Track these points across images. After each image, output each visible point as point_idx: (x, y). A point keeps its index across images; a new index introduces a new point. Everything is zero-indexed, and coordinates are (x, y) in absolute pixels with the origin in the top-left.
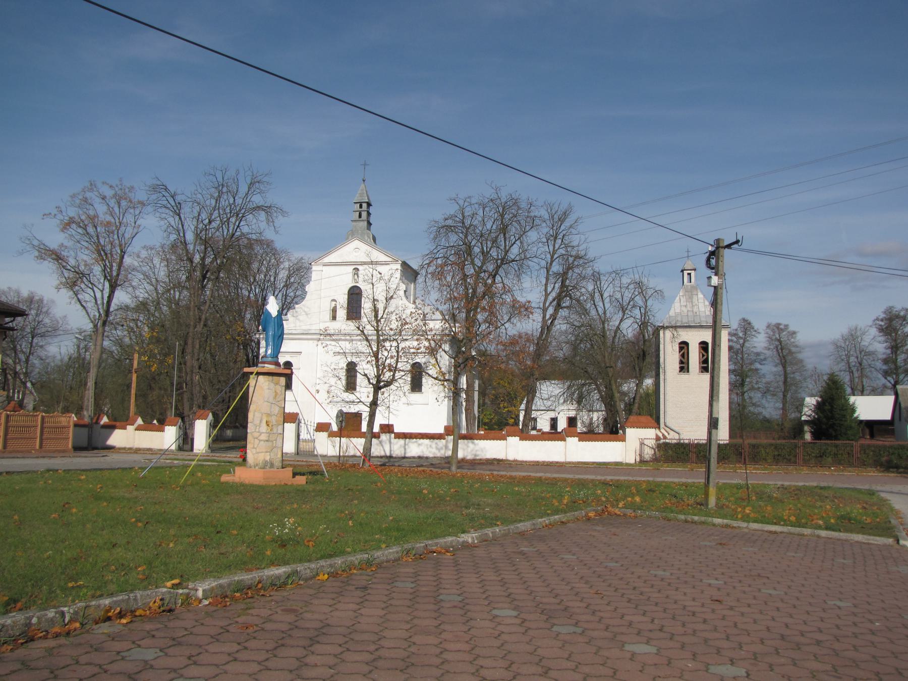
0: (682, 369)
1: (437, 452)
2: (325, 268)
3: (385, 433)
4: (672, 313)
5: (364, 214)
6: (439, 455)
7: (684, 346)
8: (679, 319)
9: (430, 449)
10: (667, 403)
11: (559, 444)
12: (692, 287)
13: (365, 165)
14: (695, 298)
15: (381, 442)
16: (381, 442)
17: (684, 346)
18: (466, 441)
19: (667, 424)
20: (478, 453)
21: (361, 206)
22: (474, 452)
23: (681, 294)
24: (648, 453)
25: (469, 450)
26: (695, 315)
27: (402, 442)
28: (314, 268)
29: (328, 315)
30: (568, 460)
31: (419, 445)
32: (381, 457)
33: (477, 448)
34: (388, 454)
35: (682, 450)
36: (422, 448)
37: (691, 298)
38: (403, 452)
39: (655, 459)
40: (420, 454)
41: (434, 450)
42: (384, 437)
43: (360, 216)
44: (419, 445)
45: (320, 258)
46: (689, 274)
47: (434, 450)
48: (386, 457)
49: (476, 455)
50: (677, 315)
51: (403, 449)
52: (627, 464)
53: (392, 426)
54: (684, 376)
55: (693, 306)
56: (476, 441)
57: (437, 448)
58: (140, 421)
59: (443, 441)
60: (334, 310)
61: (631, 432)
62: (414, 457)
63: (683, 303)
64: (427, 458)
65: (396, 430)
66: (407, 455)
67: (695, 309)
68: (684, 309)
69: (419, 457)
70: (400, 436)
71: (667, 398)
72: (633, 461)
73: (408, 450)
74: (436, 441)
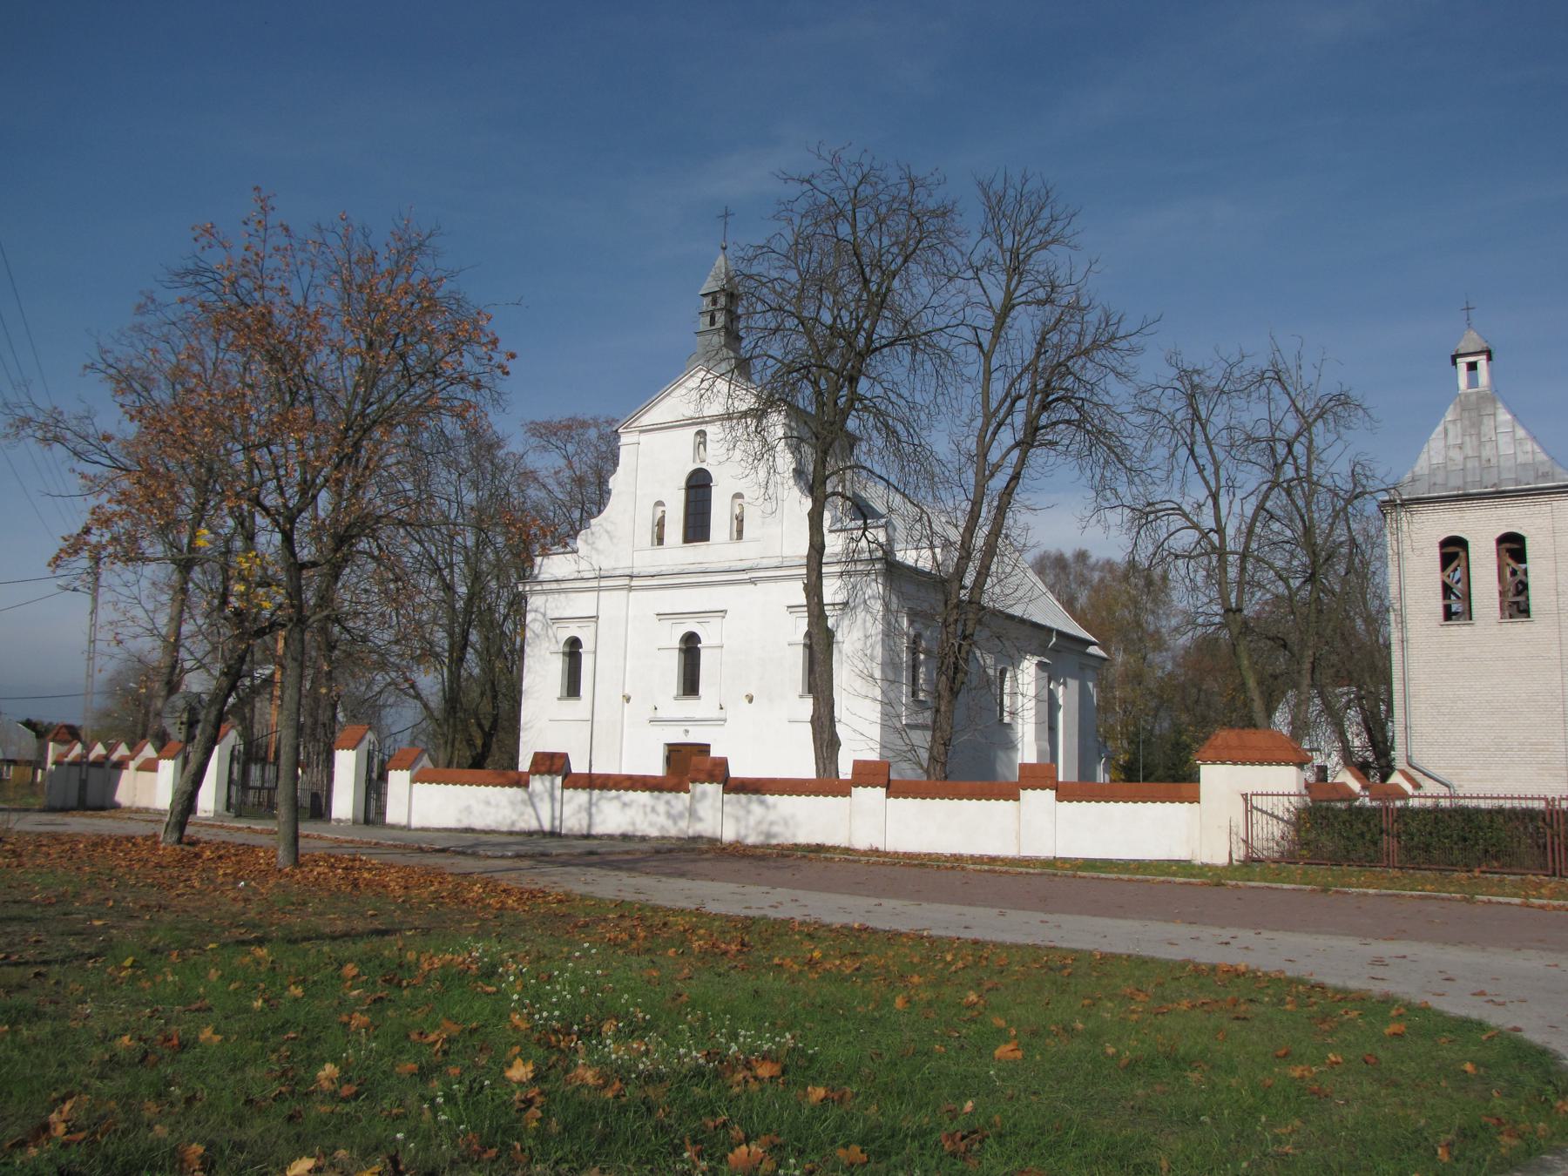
0: (1449, 615)
1: (668, 824)
2: (644, 438)
3: (542, 773)
4: (1421, 466)
5: (721, 319)
6: (673, 831)
7: (1453, 550)
8: (1439, 479)
9: (653, 817)
10: (1413, 703)
11: (999, 809)
12: (1482, 398)
13: (727, 215)
14: (1488, 423)
15: (531, 796)
16: (531, 796)
17: (1453, 550)
18: (743, 797)
19: (1415, 761)
20: (775, 829)
21: (714, 302)
22: (764, 827)
23: (1449, 416)
24: (1269, 833)
25: (752, 821)
26: (1486, 466)
27: (582, 797)
28: (624, 439)
29: (646, 534)
30: (1028, 852)
31: (625, 805)
32: (530, 834)
33: (772, 816)
34: (547, 827)
35: (1359, 826)
36: (630, 812)
37: (1477, 424)
38: (585, 823)
39: (1288, 858)
40: (629, 829)
41: (662, 820)
42: (538, 784)
43: (712, 322)
44: (625, 805)
45: (636, 417)
46: (1472, 367)
47: (662, 820)
48: (542, 834)
49: (769, 835)
50: (1433, 472)
51: (584, 815)
52: (1205, 869)
53: (565, 757)
54: (1457, 631)
55: (1481, 444)
56: (768, 797)
57: (669, 815)
58: (425, 761)
59: (685, 797)
60: (661, 524)
61: (1217, 779)
62: (611, 837)
63: (1451, 441)
64: (644, 839)
65: (735, 772)
66: (598, 829)
67: (1487, 452)
68: (1456, 455)
69: (625, 837)
70: (574, 781)
71: (1412, 689)
72: (1221, 859)
73: (597, 819)
74: (667, 796)
